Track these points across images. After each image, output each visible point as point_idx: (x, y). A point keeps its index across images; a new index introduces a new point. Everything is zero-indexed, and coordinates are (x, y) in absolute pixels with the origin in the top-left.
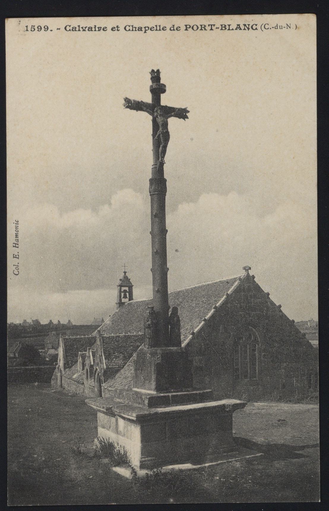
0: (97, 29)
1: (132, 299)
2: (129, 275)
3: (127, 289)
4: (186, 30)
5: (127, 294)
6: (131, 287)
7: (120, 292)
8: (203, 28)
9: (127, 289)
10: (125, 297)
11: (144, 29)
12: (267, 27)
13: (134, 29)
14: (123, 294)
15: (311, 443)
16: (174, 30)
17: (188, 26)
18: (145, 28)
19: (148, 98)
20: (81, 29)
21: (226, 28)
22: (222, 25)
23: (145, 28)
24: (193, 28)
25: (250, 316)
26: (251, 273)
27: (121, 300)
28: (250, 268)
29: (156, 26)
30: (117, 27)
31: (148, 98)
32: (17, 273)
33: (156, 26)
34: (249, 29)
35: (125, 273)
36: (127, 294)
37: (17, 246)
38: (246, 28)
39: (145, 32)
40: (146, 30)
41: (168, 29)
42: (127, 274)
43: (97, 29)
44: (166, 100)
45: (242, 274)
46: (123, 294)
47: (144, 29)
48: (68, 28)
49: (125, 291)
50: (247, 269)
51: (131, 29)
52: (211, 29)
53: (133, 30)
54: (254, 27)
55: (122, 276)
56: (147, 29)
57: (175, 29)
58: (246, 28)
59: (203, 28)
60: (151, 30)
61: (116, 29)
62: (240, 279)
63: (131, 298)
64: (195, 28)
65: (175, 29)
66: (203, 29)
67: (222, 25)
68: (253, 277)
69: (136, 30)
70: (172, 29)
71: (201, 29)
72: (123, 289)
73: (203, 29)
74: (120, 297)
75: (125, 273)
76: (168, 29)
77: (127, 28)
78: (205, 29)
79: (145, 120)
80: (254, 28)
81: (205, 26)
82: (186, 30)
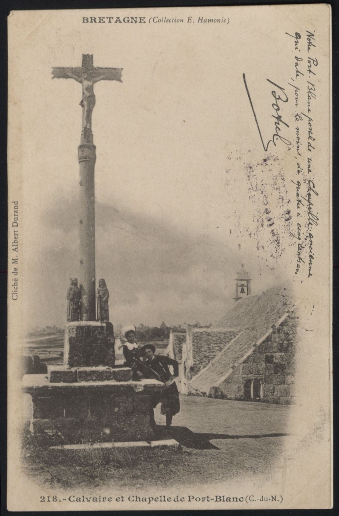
0: (102, 500)
4: (190, 501)
8: (101, 20)
11: (148, 500)
12: (252, 498)
13: (138, 500)
16: (178, 501)
17: (191, 497)
18: (149, 498)
20: (86, 500)
22: (217, 497)
23: (149, 498)
24: (196, 499)
29: (161, 497)
30: (122, 497)
32: (155, 21)
33: (161, 497)
34: (136, 22)
37: (200, 21)
38: (133, 21)
39: (149, 503)
40: (150, 501)
41: (172, 499)
43: (102, 500)
47: (148, 500)
48: (72, 499)
49: (242, 285)
51: (135, 500)
53: (136, 501)
54: (241, 500)
56: (151, 499)
57: (179, 500)
58: (133, 21)
59: (101, 20)
60: (155, 500)
61: (121, 499)
64: (198, 499)
65: (179, 500)
67: (217, 497)
69: (237, 501)
70: (176, 500)
71: (92, 22)
74: (237, 292)
76: (172, 499)
77: (131, 499)
78: (95, 22)
80: (126, 21)
81: (95, 18)
82: (190, 501)
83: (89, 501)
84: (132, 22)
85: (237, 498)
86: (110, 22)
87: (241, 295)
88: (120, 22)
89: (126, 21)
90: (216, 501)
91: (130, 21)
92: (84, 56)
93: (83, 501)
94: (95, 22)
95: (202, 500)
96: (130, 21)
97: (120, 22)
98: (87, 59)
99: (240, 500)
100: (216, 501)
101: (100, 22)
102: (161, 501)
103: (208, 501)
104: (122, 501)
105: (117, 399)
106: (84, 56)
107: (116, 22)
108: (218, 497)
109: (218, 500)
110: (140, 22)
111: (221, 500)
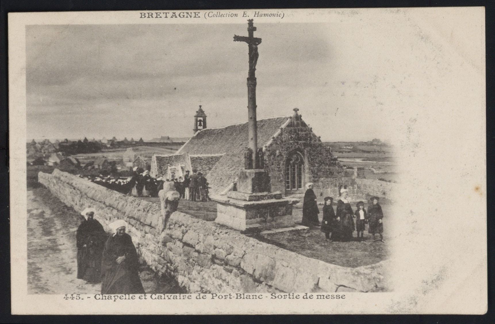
1: (206, 127)
2: (203, 108)
3: (202, 119)
4: (213, 298)
5: (202, 123)
6: (205, 118)
7: (197, 121)
9: (202, 119)
10: (200, 125)
14: (198, 123)
15: (297, 210)
16: (307, 298)
19: (247, 35)
21: (145, 17)
25: (298, 144)
26: (299, 113)
27: (197, 127)
28: (298, 110)
31: (247, 35)
34: (191, 17)
35: (200, 106)
36: (202, 123)
37: (256, 15)
38: (188, 16)
42: (202, 108)
44: (256, 35)
45: (292, 114)
46: (198, 123)
49: (200, 121)
50: (296, 110)
51: (101, 298)
52: (166, 17)
55: (198, 109)
58: (188, 16)
62: (291, 118)
63: (205, 126)
65: (308, 297)
66: (150, 16)
67: (237, 294)
68: (301, 116)
72: (199, 119)
73: (150, 16)
75: (200, 106)
78: (152, 17)
79: (245, 46)
80: (182, 16)
82: (213, 298)
83: (169, 299)
84: (187, 17)
85: (323, 296)
86: (166, 17)
87: (199, 128)
88: (176, 17)
89: (182, 16)
90: (237, 298)
91: (186, 16)
92: (261, 39)
93: (164, 299)
94: (152, 17)
95: (224, 297)
96: (186, 16)
97: (176, 17)
98: (259, 41)
99: (310, 297)
100: (237, 298)
101: (157, 17)
102: (126, 299)
103: (230, 298)
104: (230, 298)
105: (280, 208)
106: (261, 39)
107: (172, 17)
108: (239, 295)
109: (239, 297)
110: (195, 17)
111: (241, 298)
